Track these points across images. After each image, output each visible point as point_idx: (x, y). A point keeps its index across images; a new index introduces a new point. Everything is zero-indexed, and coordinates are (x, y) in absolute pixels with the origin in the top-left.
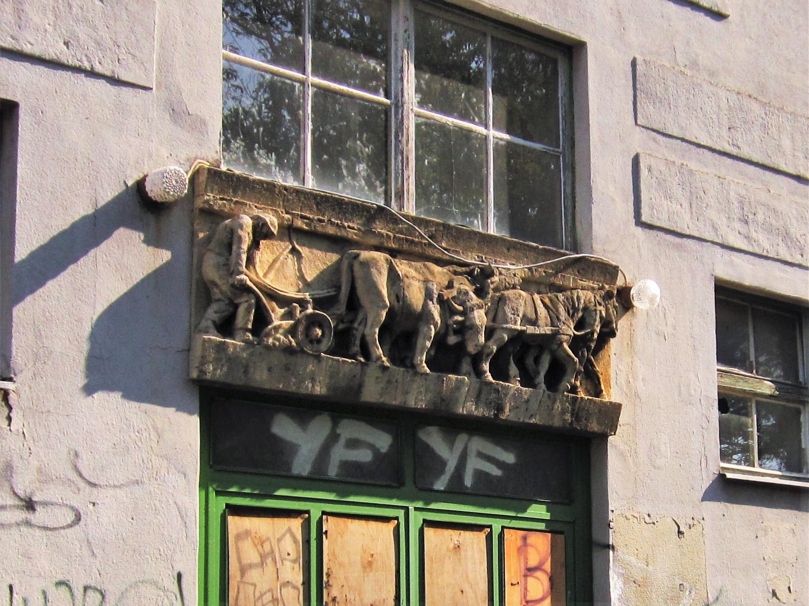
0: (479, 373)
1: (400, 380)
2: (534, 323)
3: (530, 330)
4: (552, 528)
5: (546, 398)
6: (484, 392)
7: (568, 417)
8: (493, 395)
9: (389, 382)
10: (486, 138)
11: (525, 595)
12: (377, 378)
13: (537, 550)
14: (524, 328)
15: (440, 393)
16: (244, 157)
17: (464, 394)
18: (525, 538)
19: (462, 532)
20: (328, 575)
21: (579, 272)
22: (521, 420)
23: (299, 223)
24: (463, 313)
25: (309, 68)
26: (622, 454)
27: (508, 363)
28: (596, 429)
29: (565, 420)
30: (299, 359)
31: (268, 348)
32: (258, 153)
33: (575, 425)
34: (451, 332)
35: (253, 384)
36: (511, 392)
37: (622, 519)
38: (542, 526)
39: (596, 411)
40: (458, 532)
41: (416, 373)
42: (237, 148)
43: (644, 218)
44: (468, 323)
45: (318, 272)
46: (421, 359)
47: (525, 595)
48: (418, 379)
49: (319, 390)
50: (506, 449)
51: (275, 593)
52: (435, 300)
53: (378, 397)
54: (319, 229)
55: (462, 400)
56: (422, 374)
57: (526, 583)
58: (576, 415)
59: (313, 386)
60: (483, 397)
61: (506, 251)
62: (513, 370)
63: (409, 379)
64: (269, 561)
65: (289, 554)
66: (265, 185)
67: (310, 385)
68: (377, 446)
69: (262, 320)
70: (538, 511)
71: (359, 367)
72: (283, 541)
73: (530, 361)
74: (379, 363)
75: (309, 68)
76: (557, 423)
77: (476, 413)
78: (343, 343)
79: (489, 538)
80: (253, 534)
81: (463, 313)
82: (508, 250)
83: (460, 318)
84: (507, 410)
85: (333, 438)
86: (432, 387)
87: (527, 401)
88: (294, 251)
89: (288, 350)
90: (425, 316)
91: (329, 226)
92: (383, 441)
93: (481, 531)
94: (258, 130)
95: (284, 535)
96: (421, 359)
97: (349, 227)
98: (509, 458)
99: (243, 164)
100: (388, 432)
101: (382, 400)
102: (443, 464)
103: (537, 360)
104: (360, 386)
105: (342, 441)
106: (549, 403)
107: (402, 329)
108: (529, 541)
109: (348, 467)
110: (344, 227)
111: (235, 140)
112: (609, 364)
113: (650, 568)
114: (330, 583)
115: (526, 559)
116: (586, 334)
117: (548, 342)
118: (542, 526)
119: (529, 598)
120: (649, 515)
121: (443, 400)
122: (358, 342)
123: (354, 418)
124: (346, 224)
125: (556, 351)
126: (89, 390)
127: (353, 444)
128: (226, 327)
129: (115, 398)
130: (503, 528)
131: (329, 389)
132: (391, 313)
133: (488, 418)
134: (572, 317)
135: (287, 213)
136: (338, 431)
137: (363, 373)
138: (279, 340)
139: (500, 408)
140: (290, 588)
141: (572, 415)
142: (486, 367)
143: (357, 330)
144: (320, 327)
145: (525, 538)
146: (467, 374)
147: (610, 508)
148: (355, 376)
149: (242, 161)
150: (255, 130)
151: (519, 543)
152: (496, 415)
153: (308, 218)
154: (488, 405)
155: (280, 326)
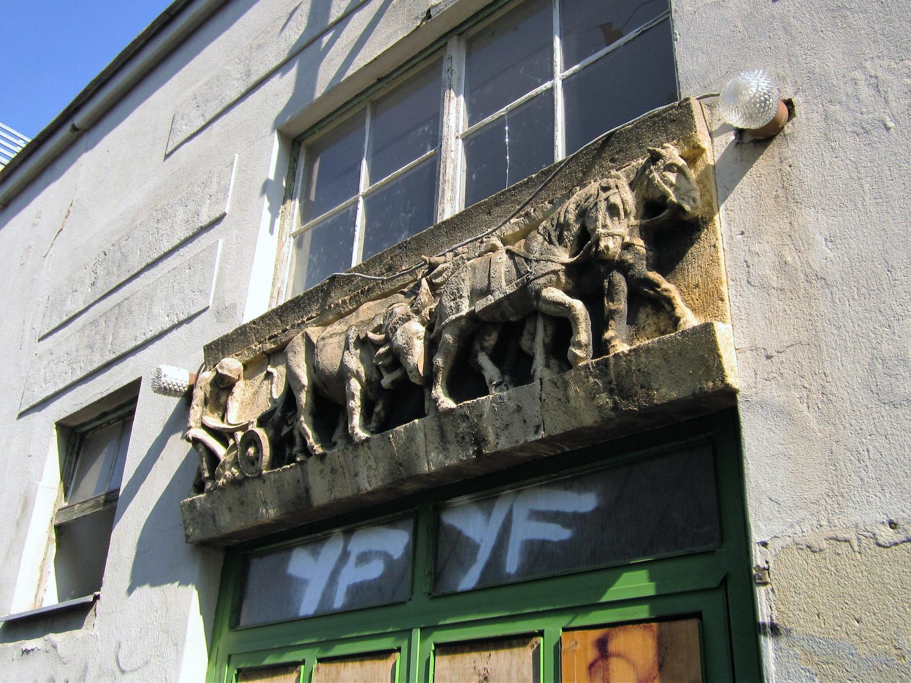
1: (343, 463)
2: (488, 291)
3: (481, 304)
4: (664, 614)
5: (548, 387)
6: (449, 429)
7: (604, 399)
8: (463, 427)
9: (333, 471)
12: (321, 472)
13: (628, 660)
15: (392, 456)
18: (602, 645)
19: (493, 653)
21: (613, 160)
22: (521, 442)
25: (548, 85)
26: (784, 413)
28: (674, 395)
29: (600, 408)
30: (248, 487)
31: (222, 489)
33: (624, 405)
34: (384, 373)
35: (224, 532)
36: (486, 409)
37: (799, 558)
38: (643, 612)
39: (657, 361)
40: (486, 654)
45: (422, 341)
48: (361, 452)
49: (270, 513)
53: (328, 494)
55: (422, 454)
58: (619, 389)
59: (267, 511)
60: (450, 436)
61: (486, 217)
62: (490, 370)
63: (351, 456)
67: (264, 511)
68: (390, 553)
70: (635, 583)
71: (299, 469)
75: (548, 85)
76: (589, 419)
77: (448, 463)
82: (489, 213)
83: (382, 350)
84: (491, 438)
86: (380, 453)
87: (519, 409)
89: (235, 483)
90: (344, 374)
92: (394, 541)
93: (524, 644)
98: (584, 502)
100: (404, 529)
102: (474, 548)
105: (352, 559)
106: (559, 394)
108: (613, 647)
109: (536, 551)
112: (714, 261)
118: (643, 612)
120: (893, 525)
121: (400, 464)
126: (316, 561)
127: (364, 558)
129: (147, 587)
131: (280, 507)
133: (467, 463)
134: (561, 240)
137: (305, 474)
139: (479, 441)
141: (611, 392)
147: (756, 537)
148: (298, 481)
151: (592, 654)
152: (479, 453)
154: (461, 441)
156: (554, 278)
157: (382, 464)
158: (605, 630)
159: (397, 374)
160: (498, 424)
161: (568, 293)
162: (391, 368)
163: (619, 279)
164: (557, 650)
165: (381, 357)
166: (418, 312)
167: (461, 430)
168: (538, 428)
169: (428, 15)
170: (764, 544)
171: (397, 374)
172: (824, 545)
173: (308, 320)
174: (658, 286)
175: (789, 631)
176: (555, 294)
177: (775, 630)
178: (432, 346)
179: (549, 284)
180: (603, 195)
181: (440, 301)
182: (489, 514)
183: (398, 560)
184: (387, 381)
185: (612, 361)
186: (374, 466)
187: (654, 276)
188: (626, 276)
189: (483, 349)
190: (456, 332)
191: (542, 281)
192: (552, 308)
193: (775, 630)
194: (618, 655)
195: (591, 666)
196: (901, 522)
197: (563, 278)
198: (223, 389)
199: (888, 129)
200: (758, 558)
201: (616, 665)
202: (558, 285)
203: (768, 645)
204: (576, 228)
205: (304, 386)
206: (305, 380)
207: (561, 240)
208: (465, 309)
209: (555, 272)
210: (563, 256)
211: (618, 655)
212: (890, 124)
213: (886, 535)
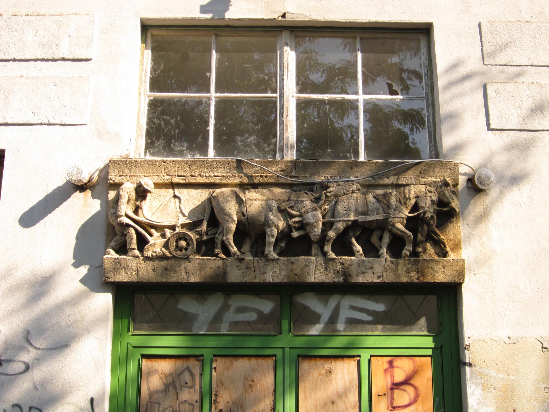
0: (325, 254)
3: (361, 219)
10: (357, 101)
11: (392, 402)
14: (357, 218)
16: (164, 148)
17: (315, 270)
18: (391, 363)
20: (216, 395)
23: (177, 180)
24: (300, 216)
27: (352, 244)
32: (174, 145)
34: (294, 230)
41: (268, 260)
42: (159, 145)
43: (492, 126)
44: (304, 222)
46: (271, 252)
47: (392, 402)
50: (377, 301)
51: (174, 408)
52: (274, 211)
54: (192, 180)
56: (273, 260)
57: (392, 394)
63: (263, 264)
64: (171, 388)
65: (186, 383)
66: (149, 162)
69: (142, 243)
72: (182, 376)
73: (374, 239)
74: (236, 257)
78: (207, 247)
79: (359, 363)
80: (160, 372)
81: (300, 216)
83: (296, 219)
85: (225, 308)
88: (175, 196)
89: (163, 258)
91: (200, 178)
94: (175, 132)
95: (183, 371)
96: (271, 252)
97: (214, 176)
99: (164, 153)
101: (244, 280)
103: (381, 239)
104: (225, 273)
105: (232, 309)
106: (393, 266)
107: (251, 232)
108: (395, 364)
110: (210, 176)
111: (158, 141)
113: (512, 377)
114: (218, 400)
115: (392, 377)
116: (419, 215)
117: (383, 226)
119: (395, 404)
120: (509, 338)
121: (296, 275)
122: (219, 246)
123: (243, 294)
124: (212, 175)
125: (391, 229)
127: (240, 310)
128: (122, 249)
130: (371, 356)
132: (239, 223)
135: (168, 175)
136: (229, 303)
138: (155, 252)
140: (186, 404)
141: (418, 272)
142: (328, 248)
143: (217, 238)
144: (185, 240)
145: (391, 363)
146: (316, 255)
149: (162, 151)
150: (173, 132)
151: (386, 366)
153: (184, 176)
155: (154, 244)
156: (402, 220)
157: (284, 272)
158: (393, 358)
159: (302, 233)
160: (359, 271)
161: (405, 227)
162: (297, 229)
163: (426, 228)
164: (369, 362)
165: (294, 222)
166: (320, 208)
167: (338, 268)
168: (379, 277)
169: (284, 16)
170: (469, 338)
171: (302, 233)
172: (488, 341)
173: (214, 176)
174: (439, 236)
175: (475, 366)
176: (400, 226)
177: (470, 365)
178: (328, 226)
179: (399, 222)
180: (429, 194)
181: (390, 231)
182: (326, 303)
183: (267, 314)
184: (295, 234)
185: (421, 261)
186: (278, 272)
187: (436, 230)
188: (428, 228)
189: (354, 236)
190: (345, 226)
191: (397, 220)
192: (400, 233)
193: (470, 365)
194: (398, 367)
195: (385, 370)
196: (512, 337)
197: (405, 221)
198: (140, 196)
199: (521, 207)
200: (466, 342)
201: (396, 370)
202: (402, 224)
203: (468, 369)
204: (413, 201)
205: (234, 221)
206: (235, 218)
207: (405, 204)
208: (352, 218)
209: (403, 218)
210: (406, 213)
211: (398, 367)
212: (522, 206)
213: (507, 341)
